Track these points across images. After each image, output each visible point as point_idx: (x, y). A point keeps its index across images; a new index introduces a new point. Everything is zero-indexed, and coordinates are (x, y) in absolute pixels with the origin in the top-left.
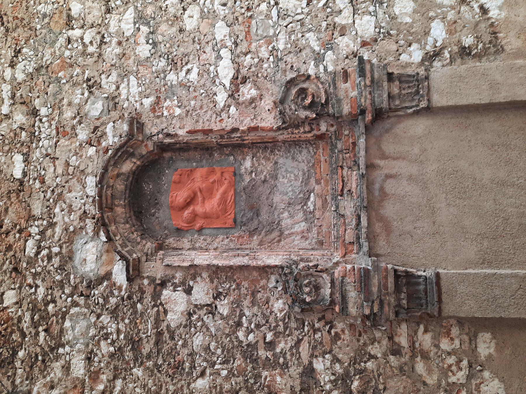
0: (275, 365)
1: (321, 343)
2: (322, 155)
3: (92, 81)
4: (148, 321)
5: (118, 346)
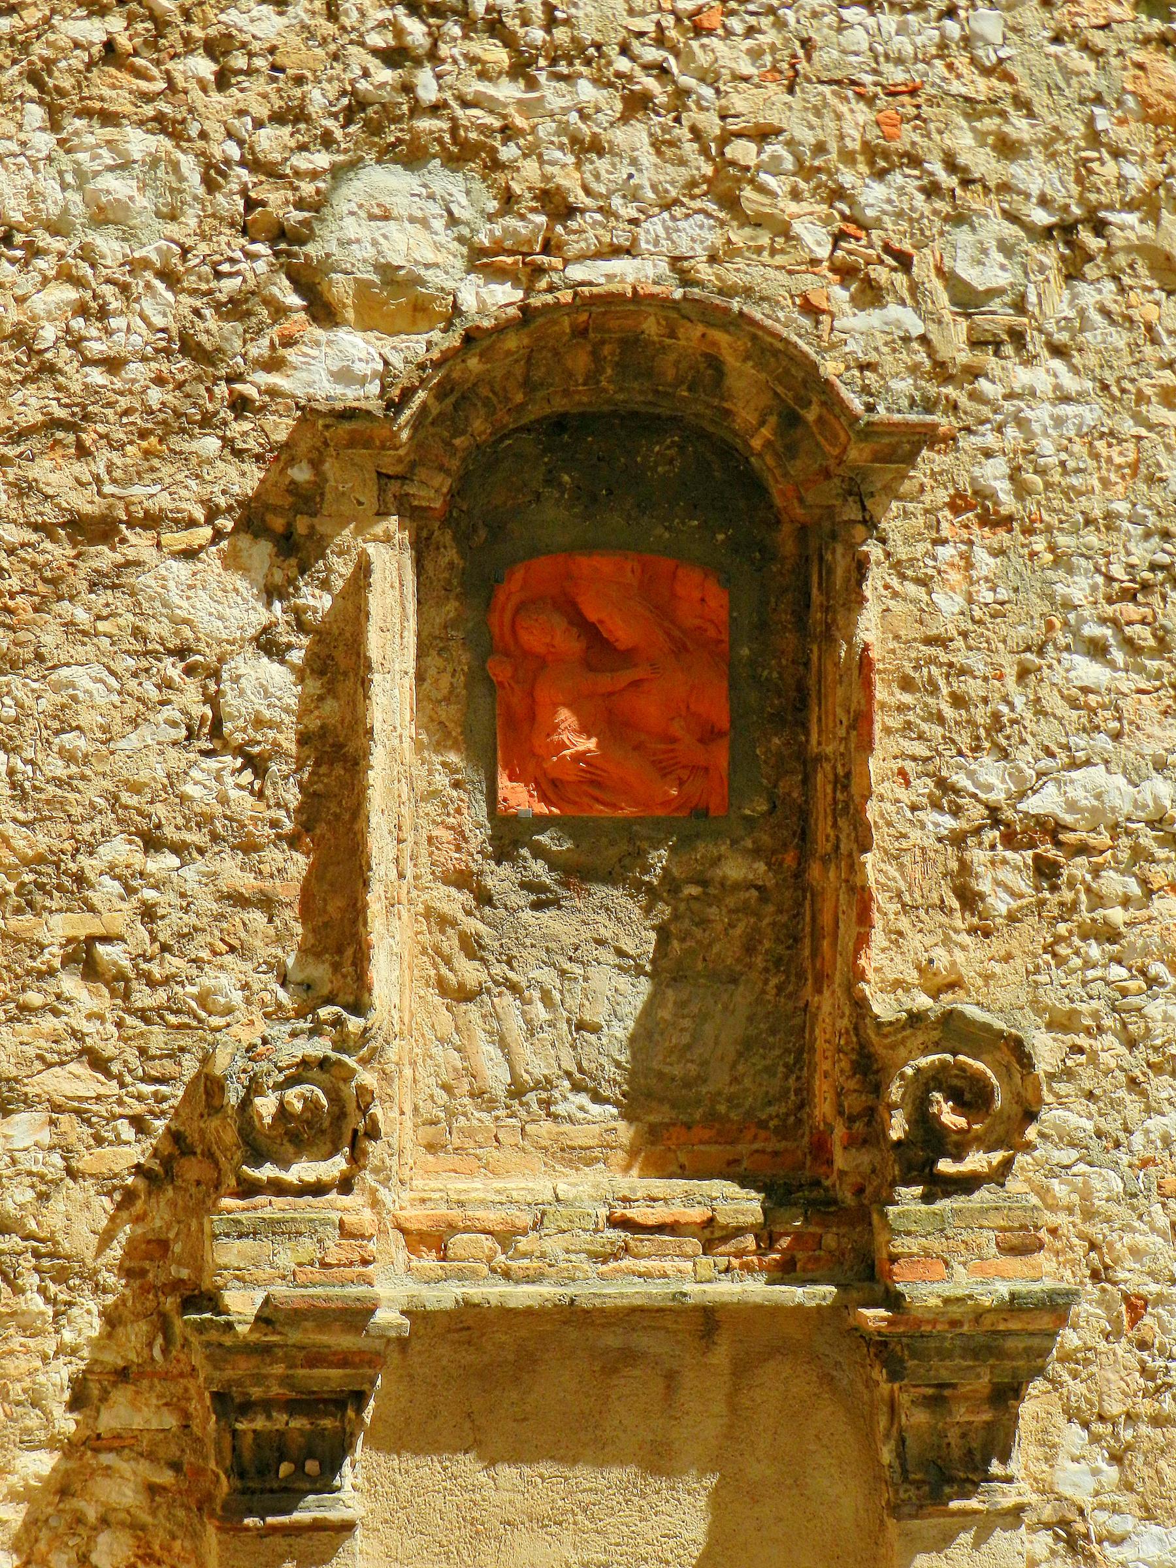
0: (17, 977)
1: (99, 1141)
2: (756, 1146)
3: (1093, 243)
4: (155, 482)
5: (61, 365)
